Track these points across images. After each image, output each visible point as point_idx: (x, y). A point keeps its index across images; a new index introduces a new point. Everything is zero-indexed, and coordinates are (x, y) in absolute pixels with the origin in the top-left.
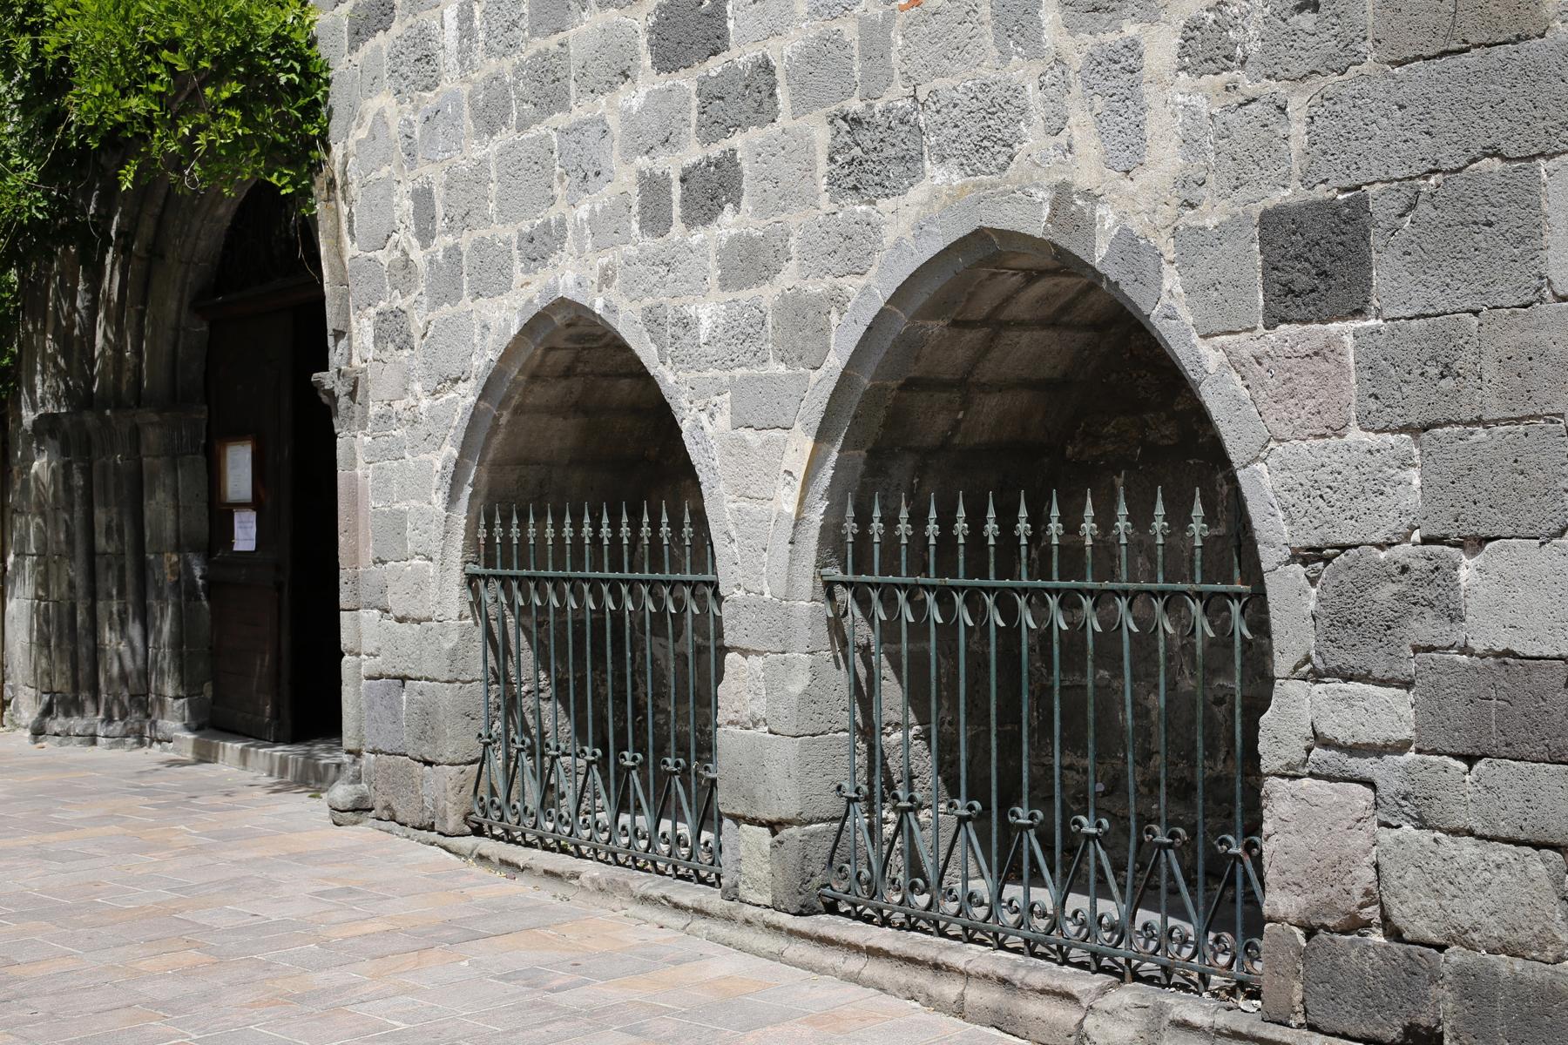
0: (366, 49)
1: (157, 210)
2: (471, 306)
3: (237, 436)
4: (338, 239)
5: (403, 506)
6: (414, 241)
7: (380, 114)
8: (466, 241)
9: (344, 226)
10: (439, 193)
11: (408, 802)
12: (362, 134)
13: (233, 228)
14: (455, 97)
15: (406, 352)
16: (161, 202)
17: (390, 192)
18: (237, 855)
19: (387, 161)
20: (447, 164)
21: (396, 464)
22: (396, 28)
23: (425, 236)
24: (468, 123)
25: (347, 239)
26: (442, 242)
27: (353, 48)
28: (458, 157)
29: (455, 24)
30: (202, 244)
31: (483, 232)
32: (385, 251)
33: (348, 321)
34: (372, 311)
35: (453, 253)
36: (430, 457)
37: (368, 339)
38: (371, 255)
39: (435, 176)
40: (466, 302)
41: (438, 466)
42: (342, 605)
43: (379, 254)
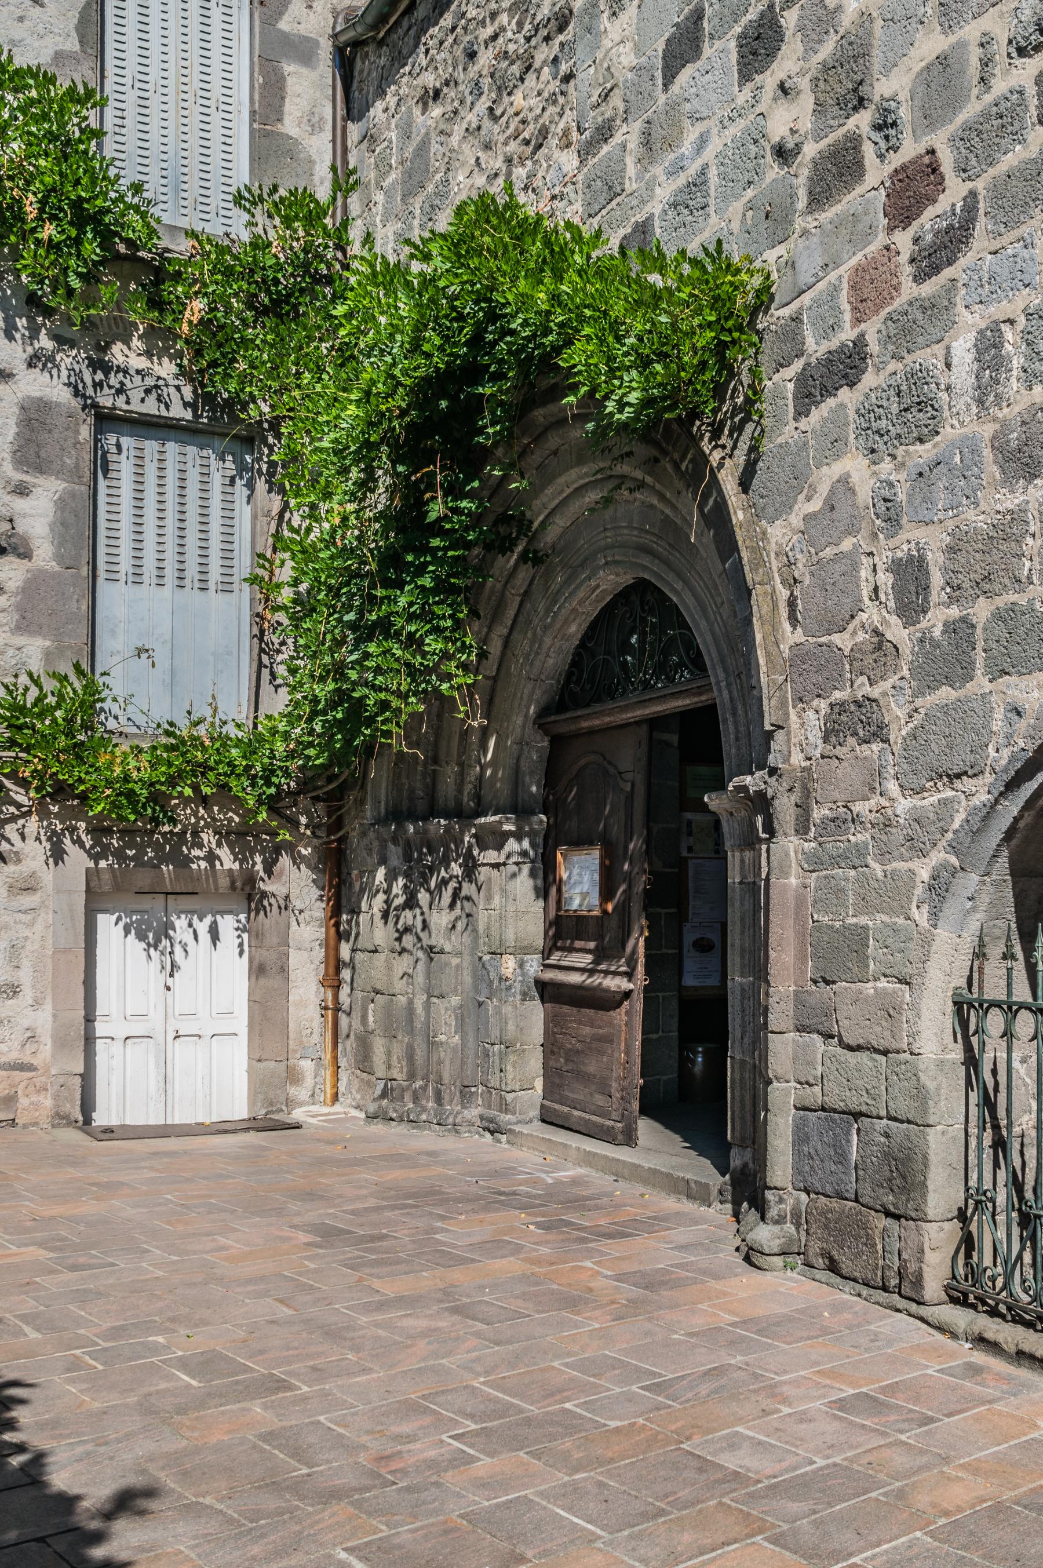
0: (817, 415)
1: (505, 631)
2: (988, 687)
3: (580, 842)
4: (775, 626)
5: (863, 920)
6: (894, 619)
7: (844, 481)
8: (982, 611)
9: (784, 612)
10: (935, 559)
11: (858, 1255)
12: (815, 505)
13: (582, 644)
14: (970, 447)
15: (876, 747)
16: (509, 623)
17: (855, 566)
18: (413, 1174)
19: (851, 531)
20: (950, 525)
21: (852, 873)
22: (870, 379)
23: (911, 610)
24: (992, 470)
25: (787, 626)
26: (937, 619)
27: (801, 413)
28: (971, 515)
29: (969, 357)
30: (551, 661)
31: (1013, 597)
32: (846, 635)
33: (787, 715)
34: (823, 705)
35: (960, 630)
36: (910, 865)
37: (815, 736)
38: (823, 640)
39: (932, 541)
40: (981, 683)
41: (925, 875)
42: (772, 1025)
43: (836, 639)
